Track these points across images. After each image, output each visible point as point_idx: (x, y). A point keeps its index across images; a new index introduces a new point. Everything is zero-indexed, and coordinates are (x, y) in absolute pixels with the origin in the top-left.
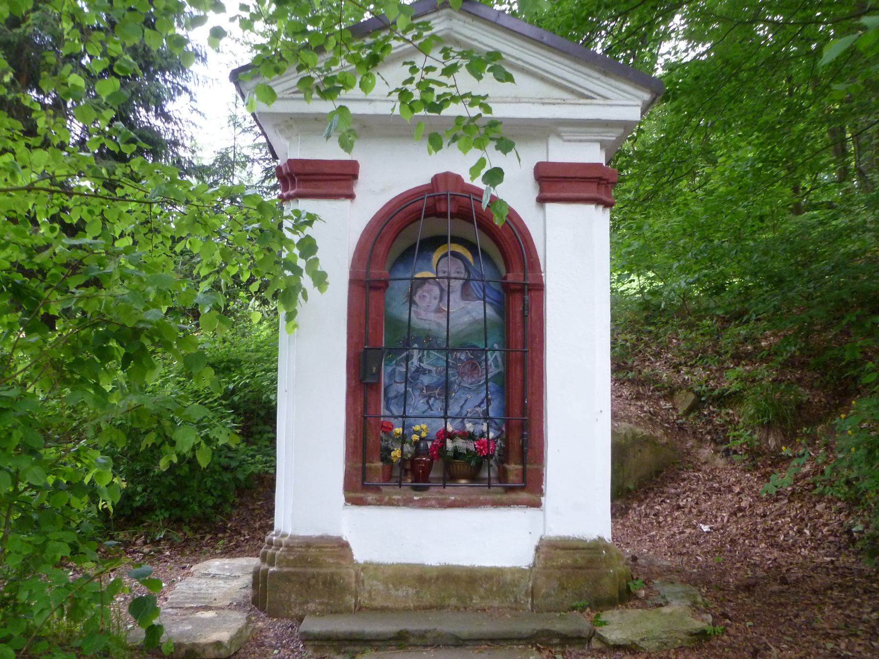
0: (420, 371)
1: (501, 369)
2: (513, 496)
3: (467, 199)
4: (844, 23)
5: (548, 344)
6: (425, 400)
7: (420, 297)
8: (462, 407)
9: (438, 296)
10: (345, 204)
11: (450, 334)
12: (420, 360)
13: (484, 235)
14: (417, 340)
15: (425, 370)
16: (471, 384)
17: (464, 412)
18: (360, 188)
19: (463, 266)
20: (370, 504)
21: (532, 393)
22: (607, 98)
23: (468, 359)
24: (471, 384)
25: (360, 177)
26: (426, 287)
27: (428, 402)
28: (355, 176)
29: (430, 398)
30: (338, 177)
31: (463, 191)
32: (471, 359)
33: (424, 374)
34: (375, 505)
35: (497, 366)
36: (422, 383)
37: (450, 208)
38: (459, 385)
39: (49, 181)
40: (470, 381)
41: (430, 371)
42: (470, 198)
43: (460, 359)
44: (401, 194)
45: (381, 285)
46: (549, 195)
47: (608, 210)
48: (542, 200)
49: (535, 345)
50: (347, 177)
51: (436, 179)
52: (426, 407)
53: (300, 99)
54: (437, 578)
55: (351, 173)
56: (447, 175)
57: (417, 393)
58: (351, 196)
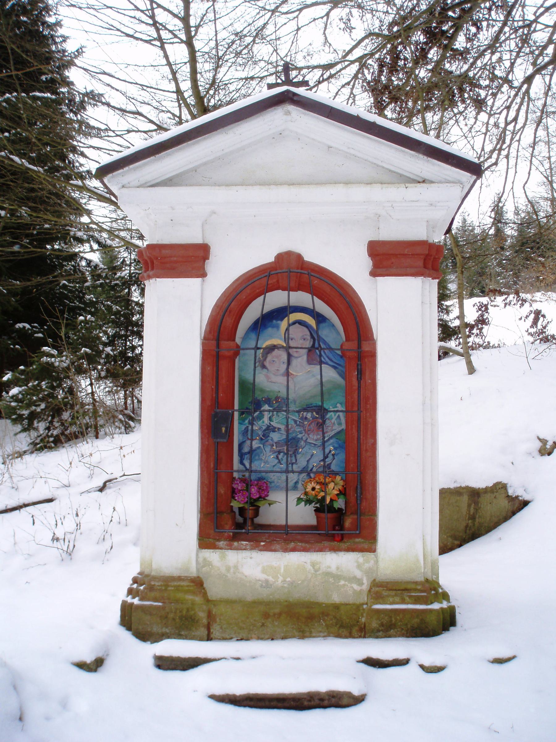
0: (270, 429)
1: (344, 427)
4: (187, 69)
5: (196, 523)
6: (275, 455)
7: (270, 362)
8: (308, 461)
9: (286, 361)
11: (324, 380)
12: (270, 419)
14: (268, 401)
15: (275, 428)
16: (316, 440)
17: (310, 467)
19: (308, 333)
21: (366, 450)
23: (314, 418)
24: (316, 440)
26: (276, 352)
27: (277, 457)
29: (279, 452)
32: (317, 418)
33: (274, 431)
35: (340, 424)
36: (272, 440)
38: (306, 441)
40: (315, 437)
41: (279, 429)
43: (306, 418)
44: (244, 275)
48: (374, 274)
49: (368, 406)
51: (280, 257)
52: (277, 461)
56: (289, 254)
57: (268, 449)
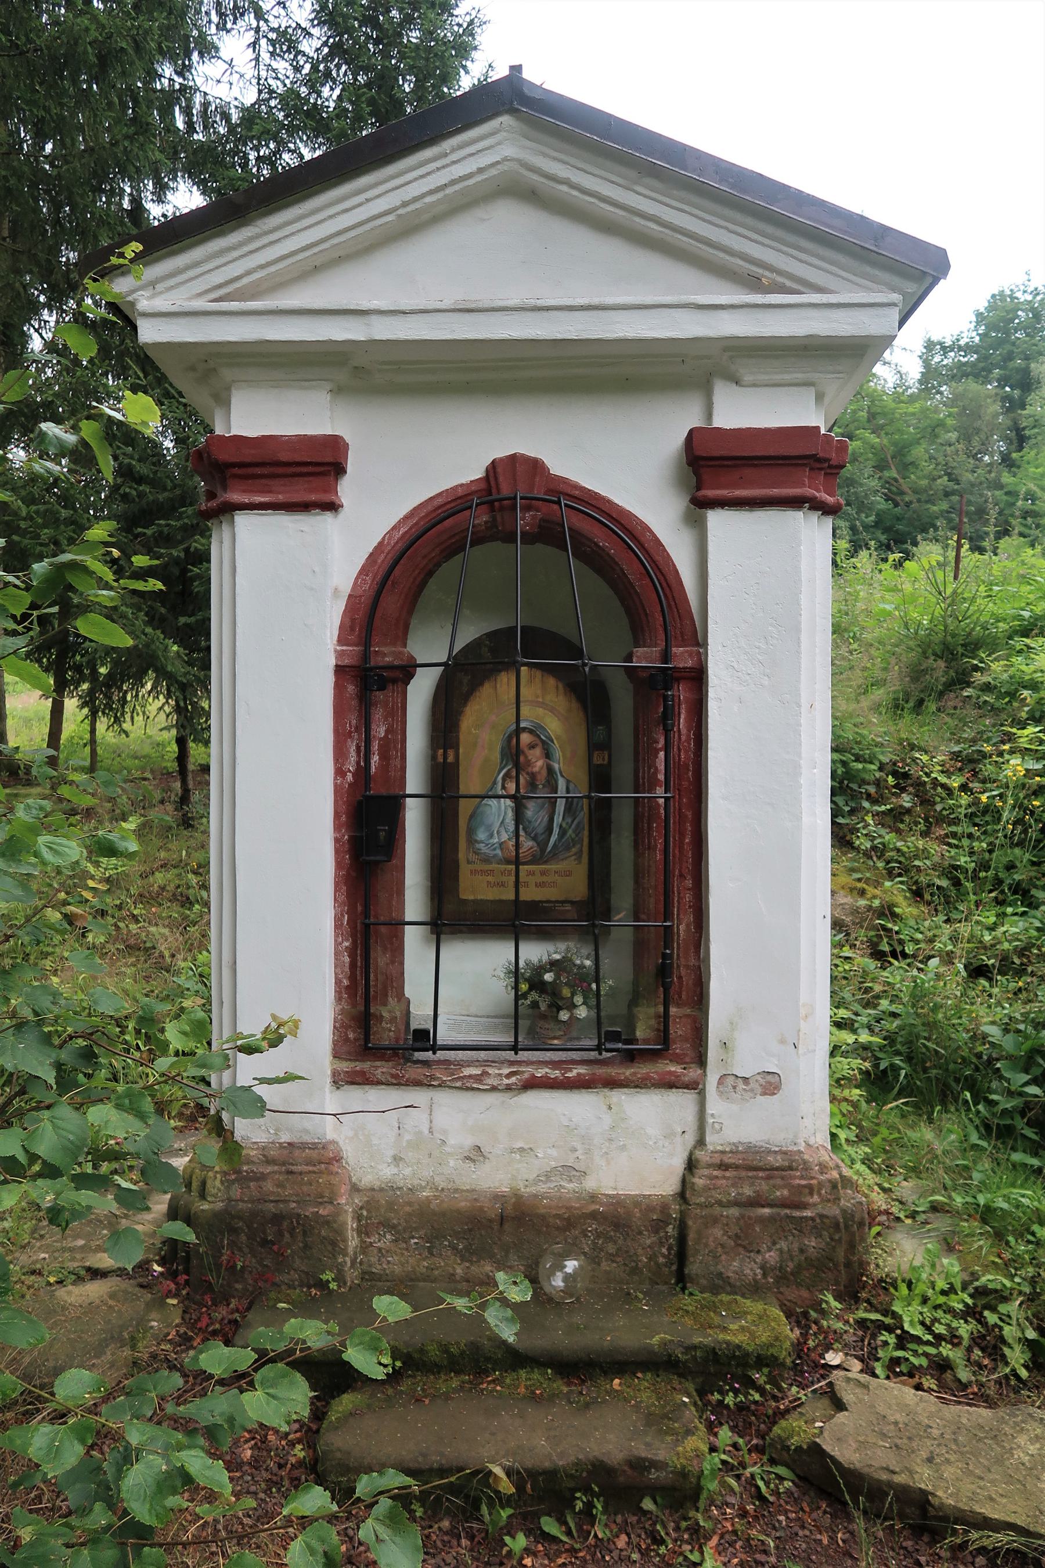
2: (642, 1069)
3: (556, 507)
10: (325, 521)
13: (586, 569)
18: (346, 490)
20: (379, 1083)
22: (830, 292)
25: (350, 468)
28: (339, 469)
30: (305, 470)
31: (549, 491)
34: (388, 1084)
37: (523, 521)
39: (51, 998)
42: (559, 503)
45: (398, 674)
46: (710, 493)
47: (828, 522)
50: (322, 469)
51: (493, 467)
53: (171, 385)
54: (502, 1219)
55: (329, 459)
58: (332, 507)
